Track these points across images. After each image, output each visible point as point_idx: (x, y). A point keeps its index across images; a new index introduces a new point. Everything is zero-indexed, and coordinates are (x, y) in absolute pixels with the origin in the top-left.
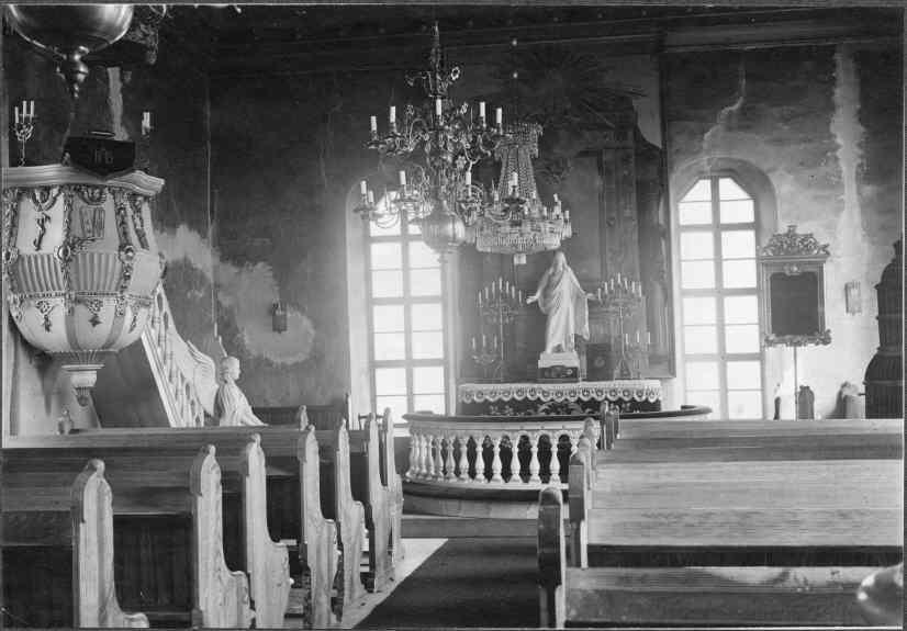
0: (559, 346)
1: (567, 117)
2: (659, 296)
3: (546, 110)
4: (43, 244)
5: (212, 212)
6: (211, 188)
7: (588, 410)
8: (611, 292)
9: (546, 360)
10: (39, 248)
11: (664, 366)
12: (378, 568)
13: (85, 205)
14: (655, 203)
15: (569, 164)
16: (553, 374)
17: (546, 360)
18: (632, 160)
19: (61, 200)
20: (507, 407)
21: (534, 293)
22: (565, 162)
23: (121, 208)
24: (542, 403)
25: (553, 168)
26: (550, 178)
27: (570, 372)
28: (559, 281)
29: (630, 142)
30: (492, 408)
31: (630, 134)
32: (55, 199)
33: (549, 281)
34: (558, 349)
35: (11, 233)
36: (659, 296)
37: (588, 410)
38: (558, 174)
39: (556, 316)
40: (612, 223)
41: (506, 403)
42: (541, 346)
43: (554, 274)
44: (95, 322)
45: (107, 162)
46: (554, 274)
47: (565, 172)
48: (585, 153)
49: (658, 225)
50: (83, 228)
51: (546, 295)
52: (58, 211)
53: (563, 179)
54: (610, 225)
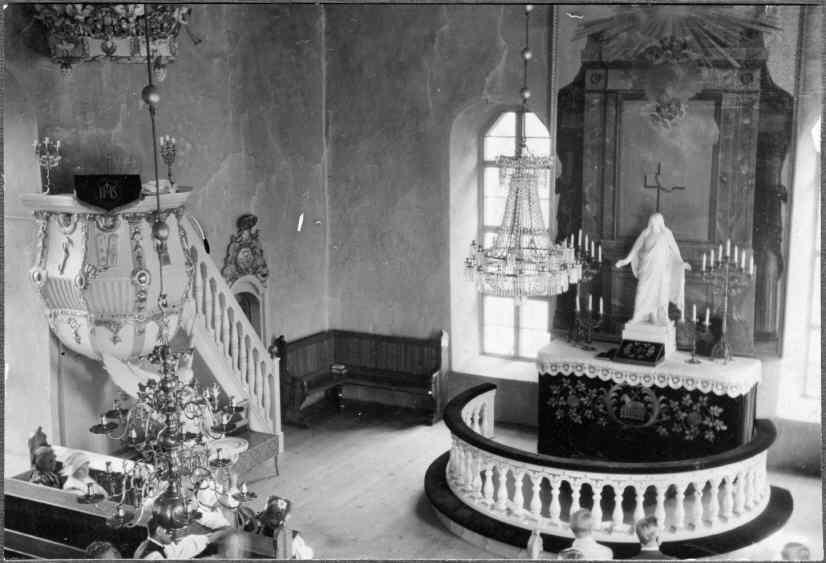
0: (650, 316)
1: (684, 51)
2: (772, 267)
3: (661, 42)
4: (65, 271)
5: (327, 134)
6: (327, 108)
7: (662, 398)
8: (717, 263)
9: (632, 331)
10: (62, 271)
11: (771, 345)
12: (500, 501)
13: (101, 232)
14: (778, 159)
15: (683, 109)
16: (627, 350)
17: (632, 331)
18: (756, 107)
19: (80, 225)
20: (579, 381)
21: (625, 255)
22: (678, 105)
23: (136, 233)
24: (614, 384)
25: (665, 111)
26: (661, 123)
27: (651, 351)
28: (655, 243)
29: (756, 85)
30: (564, 380)
31: (757, 74)
32: (75, 225)
33: (644, 246)
34: (650, 320)
35: (42, 255)
36: (772, 267)
37: (662, 398)
38: (670, 118)
39: (647, 283)
40: (725, 179)
41: (578, 378)
42: (627, 313)
43: (649, 236)
44: (115, 340)
45: (112, 196)
46: (649, 236)
47: (678, 117)
48: (702, 96)
49: (780, 186)
50: (98, 255)
51: (640, 259)
52: (78, 236)
53: (674, 125)
54: (722, 181)
